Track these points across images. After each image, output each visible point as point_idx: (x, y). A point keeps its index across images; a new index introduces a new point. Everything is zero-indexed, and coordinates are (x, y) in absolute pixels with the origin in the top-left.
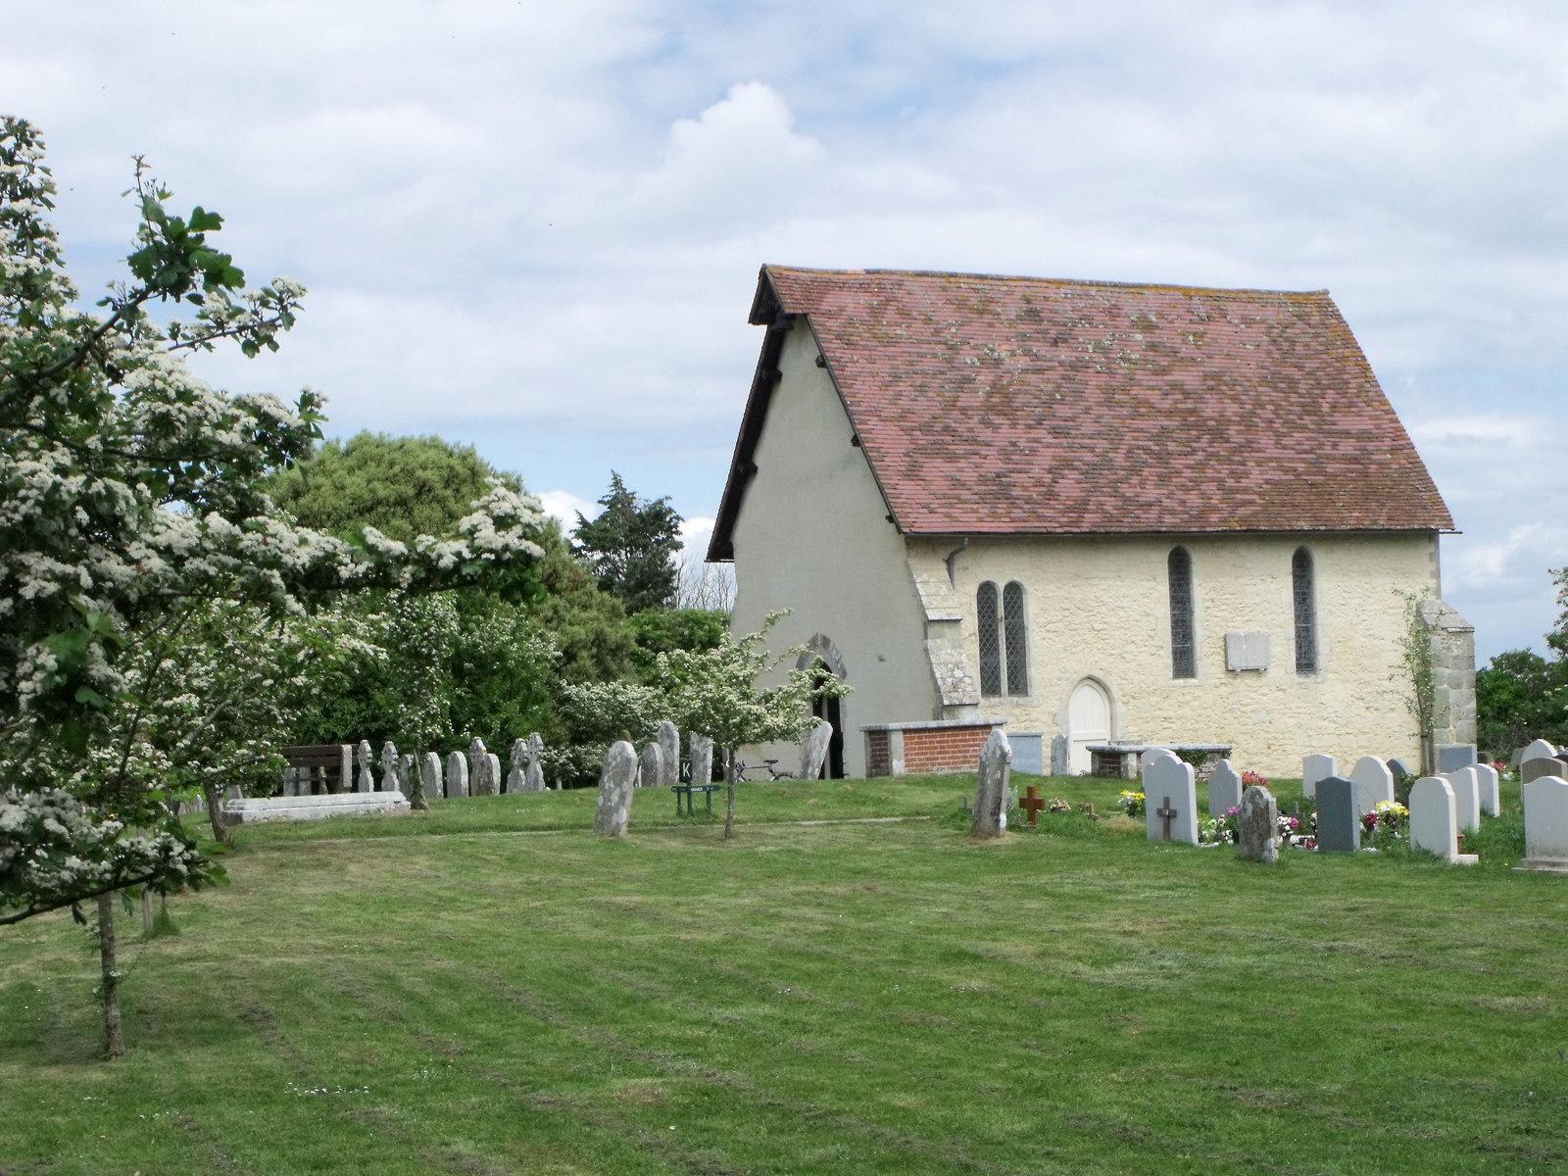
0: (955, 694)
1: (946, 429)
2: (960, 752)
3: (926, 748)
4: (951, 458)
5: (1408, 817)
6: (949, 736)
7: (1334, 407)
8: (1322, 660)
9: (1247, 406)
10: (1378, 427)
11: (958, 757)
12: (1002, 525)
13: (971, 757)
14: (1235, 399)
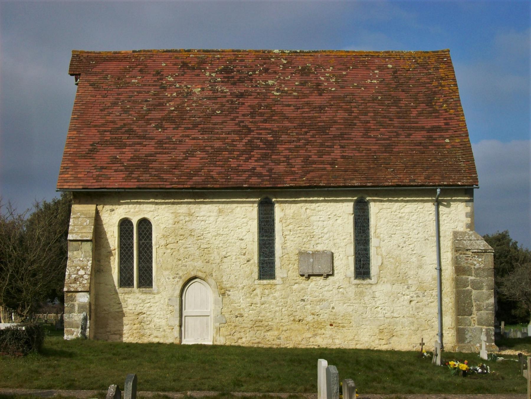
8: (374, 269)
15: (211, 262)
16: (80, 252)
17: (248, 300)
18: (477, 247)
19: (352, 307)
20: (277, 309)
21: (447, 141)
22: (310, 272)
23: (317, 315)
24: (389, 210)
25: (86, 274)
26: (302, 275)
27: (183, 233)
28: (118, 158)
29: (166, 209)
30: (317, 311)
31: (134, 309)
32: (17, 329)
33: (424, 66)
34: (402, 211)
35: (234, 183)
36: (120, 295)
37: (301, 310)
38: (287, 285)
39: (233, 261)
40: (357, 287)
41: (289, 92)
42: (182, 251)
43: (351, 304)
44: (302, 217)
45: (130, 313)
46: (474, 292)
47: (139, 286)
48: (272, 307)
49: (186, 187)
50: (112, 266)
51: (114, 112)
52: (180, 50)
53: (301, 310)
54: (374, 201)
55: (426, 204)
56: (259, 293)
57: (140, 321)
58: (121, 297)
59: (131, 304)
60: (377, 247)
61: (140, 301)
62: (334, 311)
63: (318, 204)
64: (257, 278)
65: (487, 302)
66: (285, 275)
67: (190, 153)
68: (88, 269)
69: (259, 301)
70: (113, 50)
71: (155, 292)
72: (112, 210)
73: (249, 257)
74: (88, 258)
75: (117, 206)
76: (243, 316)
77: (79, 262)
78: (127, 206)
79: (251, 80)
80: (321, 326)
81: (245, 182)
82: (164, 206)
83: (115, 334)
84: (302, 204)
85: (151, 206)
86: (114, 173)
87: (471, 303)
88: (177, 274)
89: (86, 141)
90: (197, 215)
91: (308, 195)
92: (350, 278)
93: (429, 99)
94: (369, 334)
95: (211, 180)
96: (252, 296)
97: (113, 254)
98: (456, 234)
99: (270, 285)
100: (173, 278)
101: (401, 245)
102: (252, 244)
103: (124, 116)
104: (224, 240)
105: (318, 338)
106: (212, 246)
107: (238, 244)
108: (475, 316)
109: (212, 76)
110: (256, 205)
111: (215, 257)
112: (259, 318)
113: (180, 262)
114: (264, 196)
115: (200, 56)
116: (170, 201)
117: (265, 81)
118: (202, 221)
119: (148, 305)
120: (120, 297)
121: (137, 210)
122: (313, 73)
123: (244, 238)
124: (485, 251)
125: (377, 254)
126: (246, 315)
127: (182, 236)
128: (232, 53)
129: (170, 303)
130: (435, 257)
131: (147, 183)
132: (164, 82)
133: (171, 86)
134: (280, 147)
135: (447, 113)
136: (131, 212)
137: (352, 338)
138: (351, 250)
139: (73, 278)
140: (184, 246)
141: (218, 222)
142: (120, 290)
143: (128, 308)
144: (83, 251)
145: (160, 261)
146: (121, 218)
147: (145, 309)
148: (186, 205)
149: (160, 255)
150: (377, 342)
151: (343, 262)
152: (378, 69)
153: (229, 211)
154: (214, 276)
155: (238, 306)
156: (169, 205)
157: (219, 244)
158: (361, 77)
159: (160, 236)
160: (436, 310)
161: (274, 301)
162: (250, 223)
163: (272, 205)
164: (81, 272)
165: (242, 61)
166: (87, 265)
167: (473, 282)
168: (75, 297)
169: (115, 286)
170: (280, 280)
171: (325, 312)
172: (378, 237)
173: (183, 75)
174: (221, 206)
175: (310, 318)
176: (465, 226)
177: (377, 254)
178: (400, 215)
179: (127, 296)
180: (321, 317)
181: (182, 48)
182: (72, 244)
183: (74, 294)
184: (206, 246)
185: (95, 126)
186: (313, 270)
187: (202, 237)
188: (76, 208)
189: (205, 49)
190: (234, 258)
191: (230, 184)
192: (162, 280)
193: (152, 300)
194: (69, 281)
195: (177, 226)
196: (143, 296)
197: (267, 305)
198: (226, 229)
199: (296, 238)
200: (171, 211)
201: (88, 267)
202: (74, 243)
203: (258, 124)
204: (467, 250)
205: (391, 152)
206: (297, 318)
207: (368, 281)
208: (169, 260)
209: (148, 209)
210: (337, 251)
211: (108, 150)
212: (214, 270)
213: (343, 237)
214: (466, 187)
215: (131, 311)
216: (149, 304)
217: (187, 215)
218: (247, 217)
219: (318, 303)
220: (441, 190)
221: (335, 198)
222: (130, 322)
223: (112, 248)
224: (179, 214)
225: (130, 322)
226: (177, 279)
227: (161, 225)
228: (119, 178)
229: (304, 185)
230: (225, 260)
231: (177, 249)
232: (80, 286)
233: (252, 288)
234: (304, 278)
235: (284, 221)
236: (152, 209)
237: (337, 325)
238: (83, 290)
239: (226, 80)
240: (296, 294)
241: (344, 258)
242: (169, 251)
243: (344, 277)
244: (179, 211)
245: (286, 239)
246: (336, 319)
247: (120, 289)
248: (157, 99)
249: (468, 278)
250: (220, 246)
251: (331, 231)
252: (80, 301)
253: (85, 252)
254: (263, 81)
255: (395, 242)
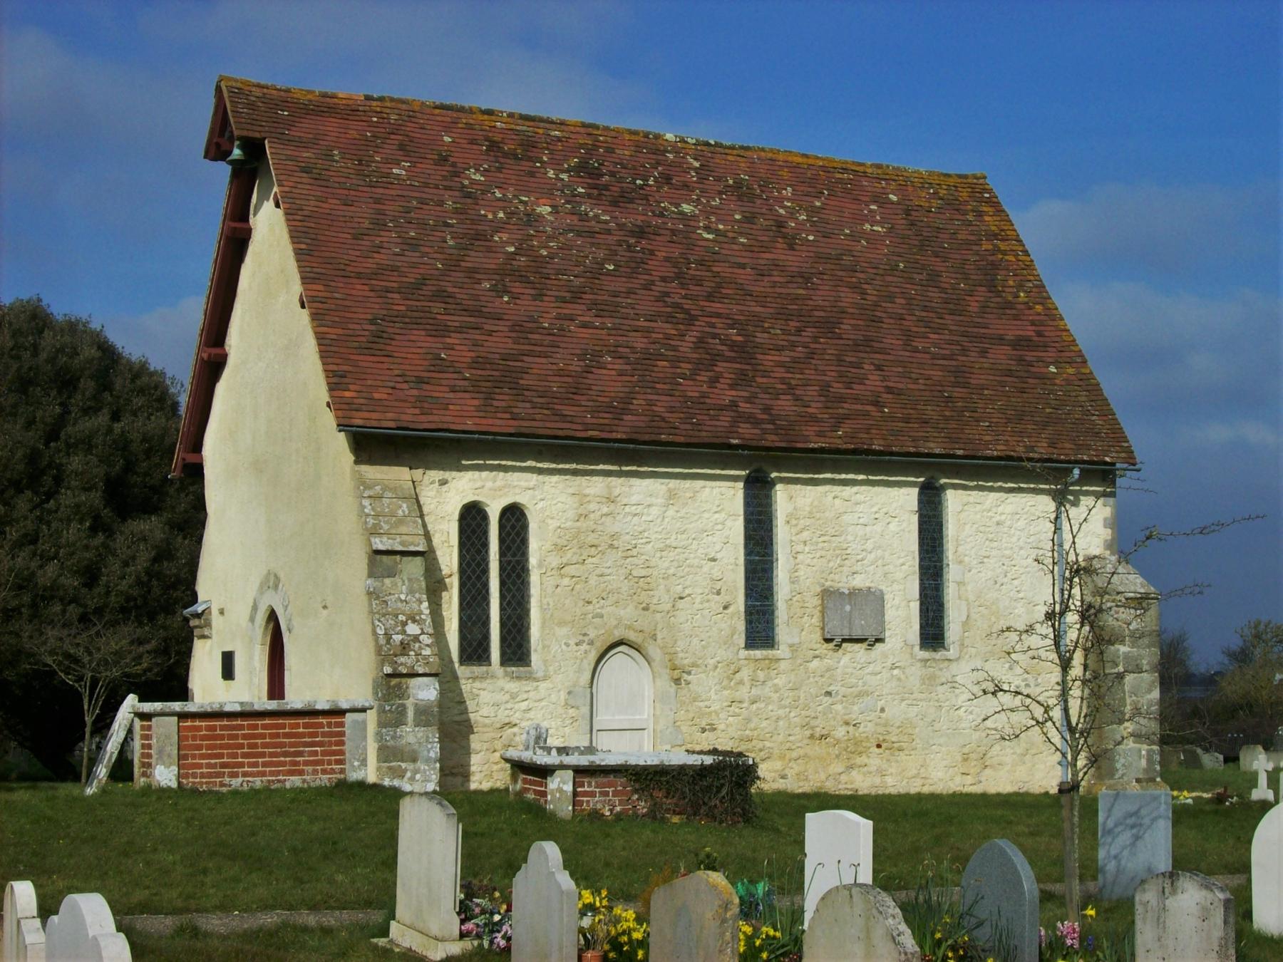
0: (402, 659)
1: (441, 295)
2: (286, 754)
3: (221, 747)
4: (441, 331)
5: (643, 943)
6: (265, 727)
7: (984, 308)
8: (953, 629)
9: (868, 297)
10: (1039, 334)
11: (283, 764)
12: (499, 422)
13: (306, 763)
14: (855, 287)
15: (652, 607)
16: (397, 579)
17: (726, 693)
18: (1132, 589)
19: (916, 709)
20: (781, 712)
21: (1053, 369)
22: (846, 633)
23: (854, 725)
24: (979, 507)
25: (423, 633)
26: (828, 641)
27: (596, 542)
28: (443, 359)
29: (561, 486)
30: (854, 717)
31: (493, 715)
32: (738, 764)
33: (953, 205)
34: (1000, 509)
35: (709, 434)
36: (462, 681)
37: (824, 714)
38: (799, 661)
39: (697, 606)
40: (925, 666)
41: (731, 235)
42: (593, 580)
43: (915, 702)
44: (827, 514)
45: (485, 726)
47: (505, 661)
48: (770, 707)
49: (619, 437)
50: (444, 613)
51: (385, 245)
52: (471, 109)
53: (824, 714)
54: (955, 487)
55: (547, 478)
56: (746, 679)
57: (507, 743)
58: (466, 686)
59: (488, 704)
60: (959, 583)
61: (507, 697)
62: (883, 715)
63: (856, 489)
64: (743, 646)
65: (1149, 697)
66: (796, 640)
67: (592, 360)
68: (425, 620)
69: (746, 696)
70: (318, 89)
71: (540, 674)
72: (443, 482)
73: (728, 598)
74: (417, 595)
75: (454, 474)
76: (715, 729)
77: (399, 604)
78: (477, 474)
79: (646, 198)
80: (861, 749)
82: (555, 478)
83: (453, 774)
84: (828, 487)
85: (529, 475)
86: (451, 395)
87: (1124, 699)
88: (585, 635)
89: (353, 310)
90: (625, 501)
91: (837, 468)
92: (913, 646)
93: (989, 277)
94: (945, 763)
95: (663, 424)
96: (732, 684)
97: (449, 586)
99: (767, 662)
100: (577, 645)
101: (1000, 580)
102: (733, 570)
103: (413, 256)
104: (678, 561)
105: (854, 773)
106: (655, 573)
107: (705, 569)
109: (563, 180)
110: (741, 485)
111: (661, 597)
112: (747, 732)
113: (591, 607)
114: (755, 466)
115: (518, 128)
116: (567, 466)
117: (677, 205)
118: (635, 515)
119: (524, 705)
120: (463, 687)
121: (499, 483)
122: (760, 197)
123: (719, 556)
125: (960, 598)
126: (722, 727)
127: (593, 549)
128: (582, 130)
129: (571, 702)
131: (534, 424)
132: (466, 182)
133: (484, 192)
135: (1031, 312)
136: (486, 488)
137: (916, 772)
138: (913, 587)
139: (398, 643)
140: (598, 572)
141: (667, 520)
142: (462, 671)
143: (480, 713)
144: (405, 578)
145: (548, 604)
146: (466, 501)
147: (517, 715)
148: (601, 479)
149: (550, 590)
150: (958, 779)
151: (900, 613)
152: (875, 202)
153: (688, 495)
154: (659, 641)
155: (706, 707)
156: (567, 477)
157: (668, 568)
158: (844, 210)
159: (548, 546)
161: (775, 696)
162: (729, 523)
163: (769, 485)
164: (412, 629)
165: (610, 150)
166: (421, 613)
168: (407, 688)
169: (451, 661)
170: (787, 650)
171: (868, 718)
172: (961, 562)
173: (499, 170)
174: (673, 483)
175: (840, 732)
176: (1102, 545)
177: (960, 598)
178: (998, 518)
179: (477, 684)
180: (861, 729)
181: (475, 104)
182: (381, 561)
183: (404, 680)
184: (643, 573)
185: (359, 276)
186: (850, 629)
187: (634, 552)
189: (523, 113)
190: (698, 600)
191: (704, 436)
192: (555, 648)
193: (531, 694)
194: (390, 650)
195: (584, 525)
196: (513, 686)
197: (763, 705)
198: (684, 536)
199: (815, 560)
200: (571, 491)
201: (423, 617)
202: (385, 558)
203: (702, 303)
204: (1118, 593)
205: (966, 385)
206: (818, 732)
207: (940, 654)
208: (567, 602)
209: (523, 484)
210: (889, 589)
211: (413, 338)
212: (659, 627)
213: (901, 561)
214: (477, 436)
215: (487, 721)
216: (526, 703)
217: (604, 500)
218: (722, 509)
219: (856, 700)
220: (1082, 470)
221: (886, 478)
222: (485, 746)
223: (445, 571)
224: (588, 499)
225: (485, 746)
226: (585, 647)
227: (550, 521)
228: (469, 408)
229: (844, 446)
230: (681, 604)
231: (583, 578)
232: (418, 661)
233: (732, 667)
234: (831, 645)
235: (794, 522)
236: (532, 484)
237: (890, 745)
238: (427, 671)
239: (595, 192)
240: (816, 679)
241: (903, 604)
242: (566, 581)
243: (902, 644)
244: (587, 491)
245: (797, 561)
246: (889, 733)
247: (463, 667)
248: (468, 222)
249: (1118, 650)
250: (671, 571)
251: (880, 547)
252: (420, 697)
253: (410, 580)
254: (671, 204)
255: (990, 574)
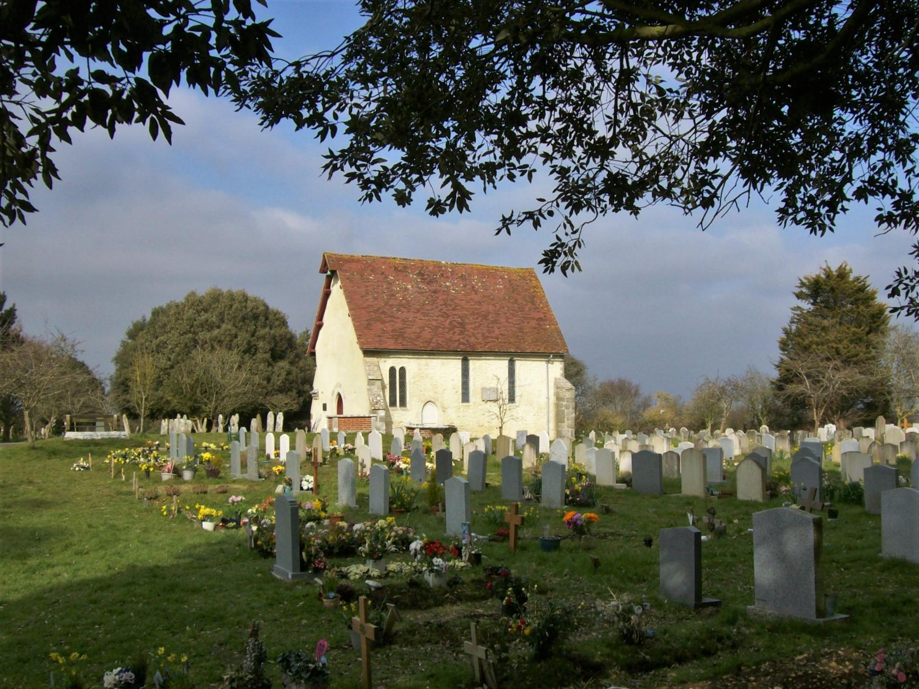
8: (517, 399)
46: (566, 411)
67: (422, 328)
81: (458, 347)
91: (486, 355)
98: (556, 379)
108: (566, 424)
124: (571, 389)
130: (546, 392)
134: (468, 327)
160: (546, 420)
164: (378, 398)
167: (565, 405)
175: (486, 424)
188: (557, 368)
191: (451, 349)
196: (403, 412)
207: (514, 404)
